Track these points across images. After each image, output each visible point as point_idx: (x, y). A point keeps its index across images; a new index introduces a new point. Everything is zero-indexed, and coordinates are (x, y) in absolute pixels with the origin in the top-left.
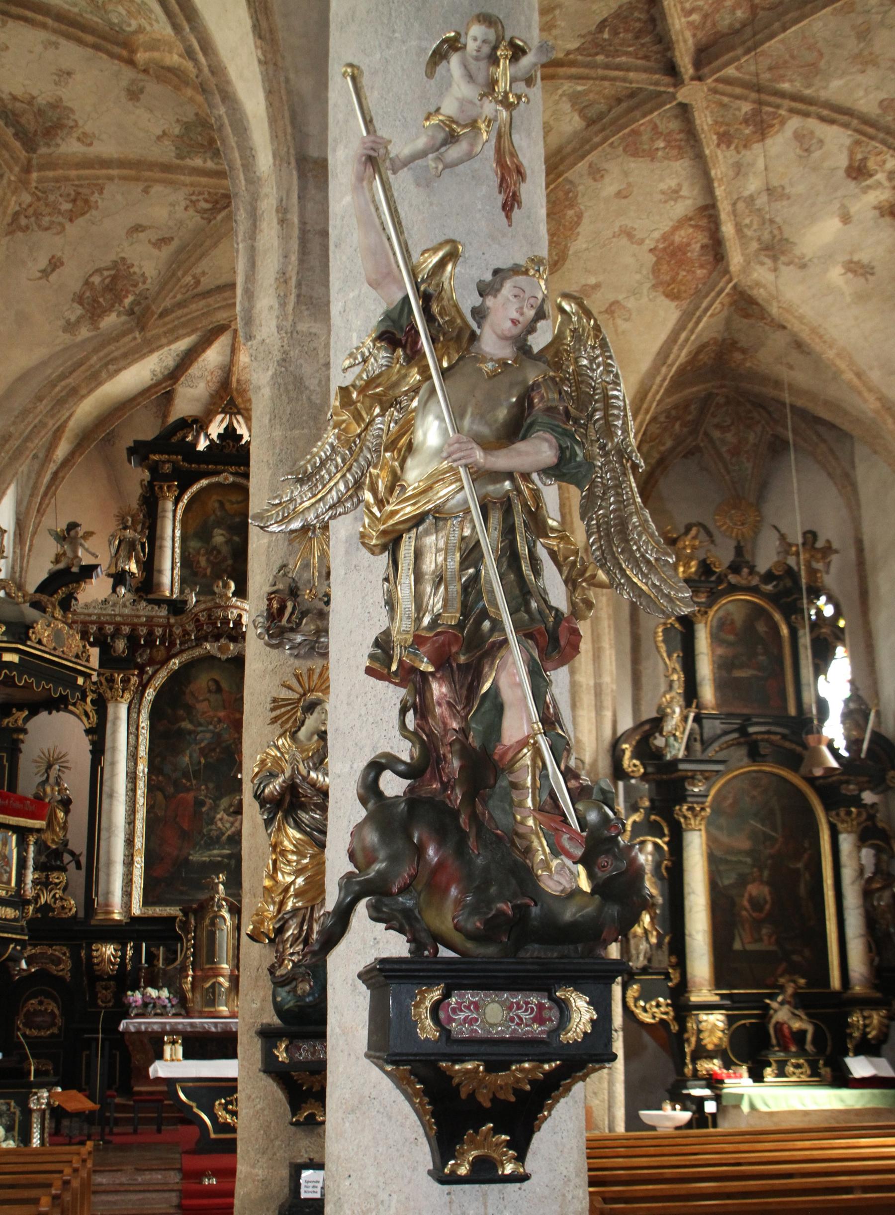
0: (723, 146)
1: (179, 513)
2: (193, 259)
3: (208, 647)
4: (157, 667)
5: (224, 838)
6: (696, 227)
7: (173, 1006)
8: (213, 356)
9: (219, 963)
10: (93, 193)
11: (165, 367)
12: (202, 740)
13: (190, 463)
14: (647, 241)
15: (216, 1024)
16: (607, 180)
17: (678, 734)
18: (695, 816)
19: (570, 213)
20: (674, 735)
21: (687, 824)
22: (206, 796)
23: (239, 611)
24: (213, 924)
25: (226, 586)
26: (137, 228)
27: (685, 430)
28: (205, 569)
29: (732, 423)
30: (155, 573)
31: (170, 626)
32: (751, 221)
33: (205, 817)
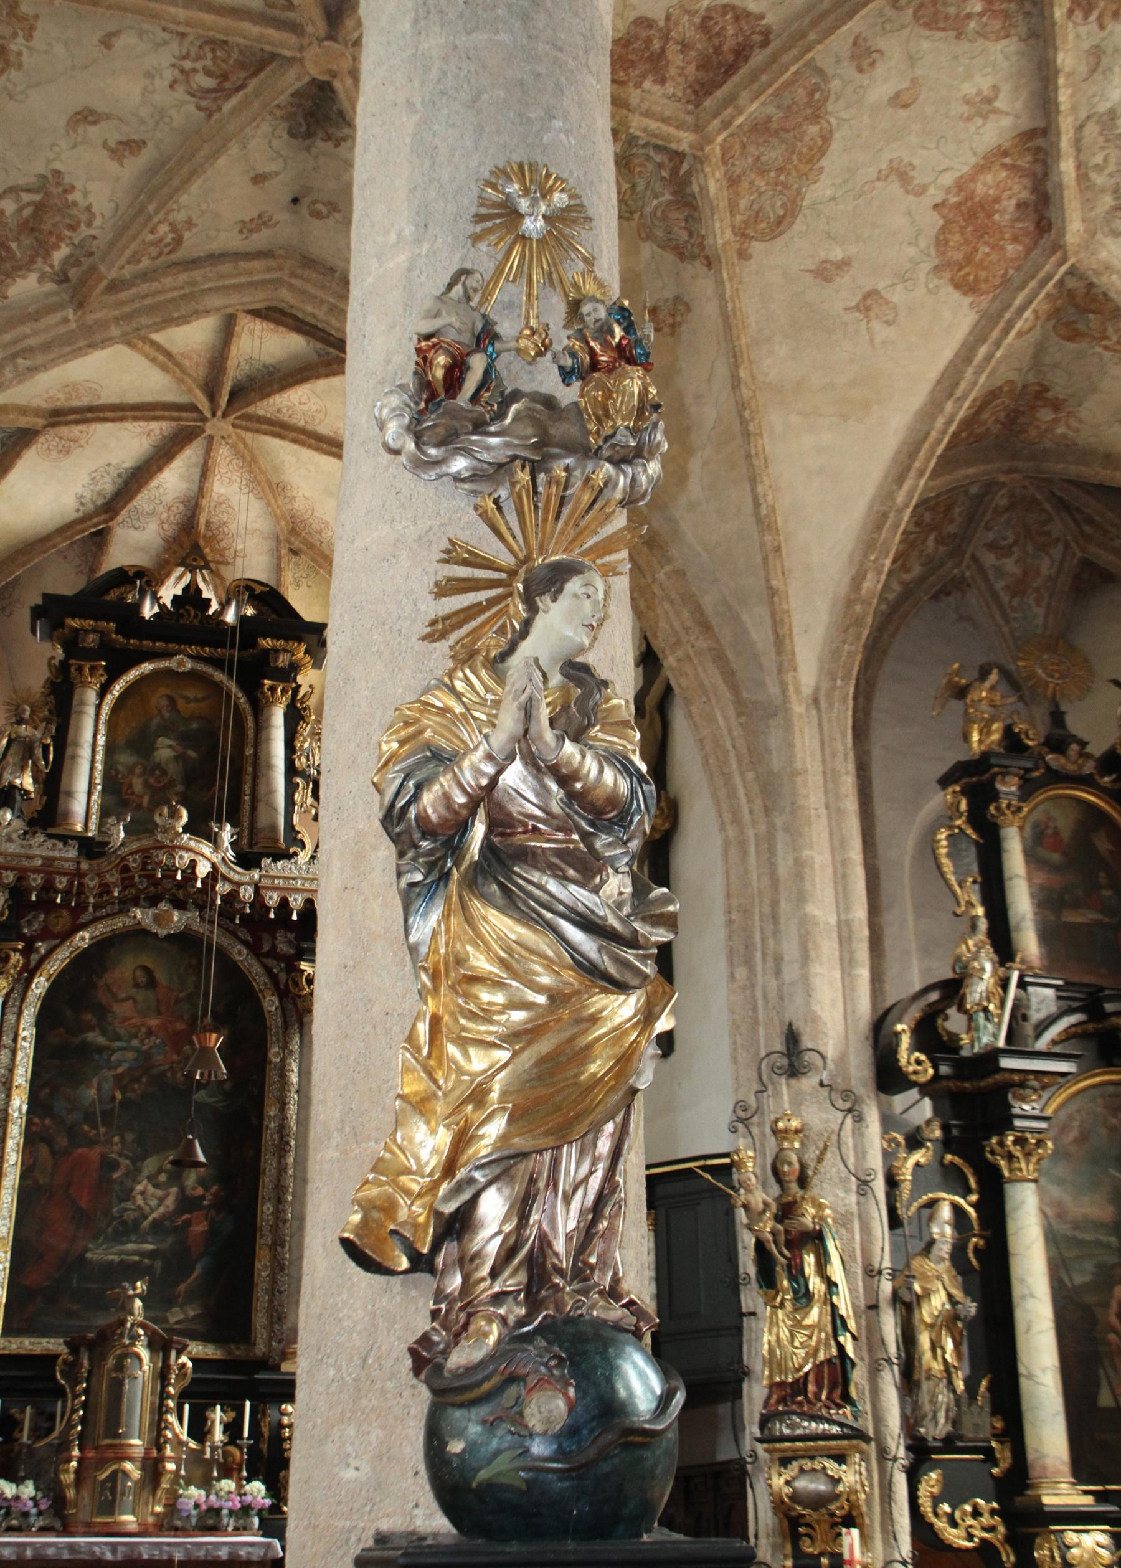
0: (1078, 14)
1: (106, 710)
2: (176, 182)
3: (139, 916)
4: (57, 942)
5: (146, 1223)
6: (1011, 168)
7: (40, 1513)
8: (173, 481)
9: (127, 1436)
10: (15, 35)
11: (99, 493)
12: (120, 1063)
13: (127, 636)
14: (931, 191)
15: (114, 1547)
16: (880, 70)
17: (991, 1007)
18: (1028, 1155)
19: (813, 130)
20: (986, 1010)
21: (1011, 1170)
22: (120, 1155)
23: (193, 856)
24: (120, 1367)
25: (174, 815)
26: (86, 116)
27: (942, 549)
28: (141, 797)
29: (1016, 542)
30: (62, 797)
31: (80, 874)
32: (1105, 160)
33: (116, 1187)
